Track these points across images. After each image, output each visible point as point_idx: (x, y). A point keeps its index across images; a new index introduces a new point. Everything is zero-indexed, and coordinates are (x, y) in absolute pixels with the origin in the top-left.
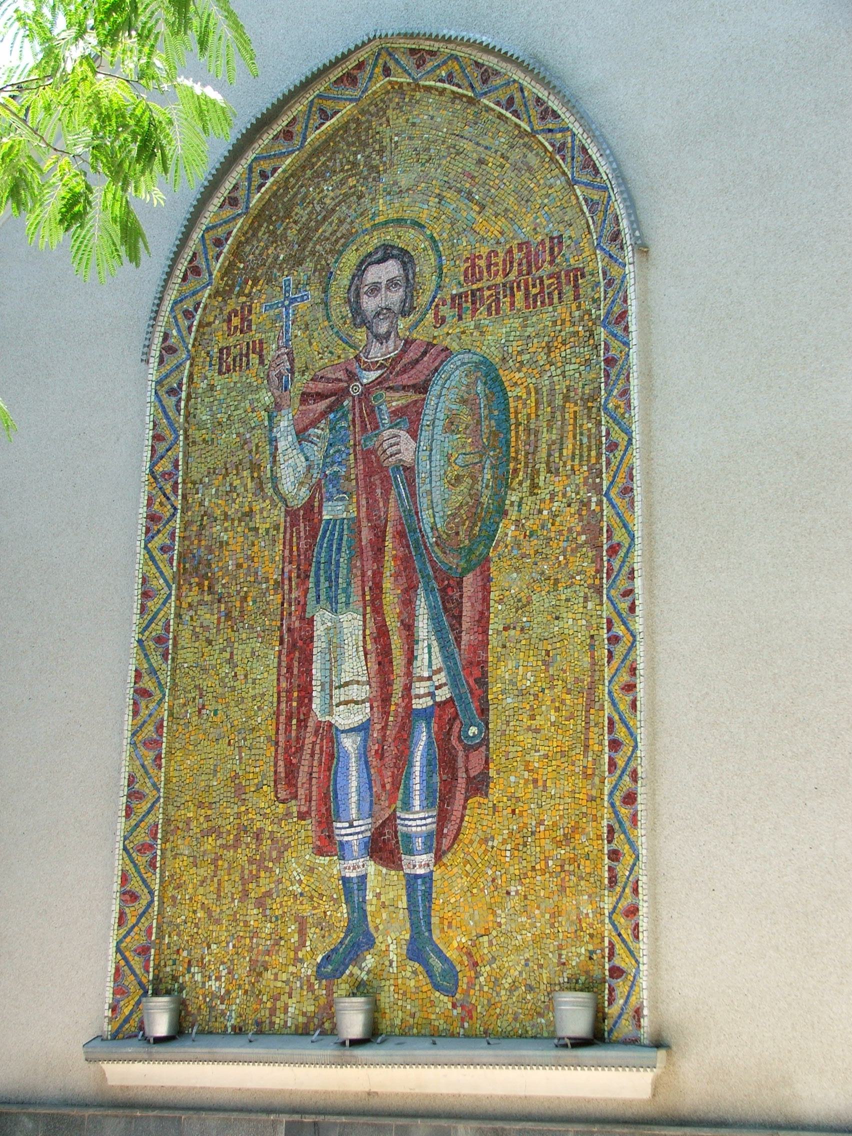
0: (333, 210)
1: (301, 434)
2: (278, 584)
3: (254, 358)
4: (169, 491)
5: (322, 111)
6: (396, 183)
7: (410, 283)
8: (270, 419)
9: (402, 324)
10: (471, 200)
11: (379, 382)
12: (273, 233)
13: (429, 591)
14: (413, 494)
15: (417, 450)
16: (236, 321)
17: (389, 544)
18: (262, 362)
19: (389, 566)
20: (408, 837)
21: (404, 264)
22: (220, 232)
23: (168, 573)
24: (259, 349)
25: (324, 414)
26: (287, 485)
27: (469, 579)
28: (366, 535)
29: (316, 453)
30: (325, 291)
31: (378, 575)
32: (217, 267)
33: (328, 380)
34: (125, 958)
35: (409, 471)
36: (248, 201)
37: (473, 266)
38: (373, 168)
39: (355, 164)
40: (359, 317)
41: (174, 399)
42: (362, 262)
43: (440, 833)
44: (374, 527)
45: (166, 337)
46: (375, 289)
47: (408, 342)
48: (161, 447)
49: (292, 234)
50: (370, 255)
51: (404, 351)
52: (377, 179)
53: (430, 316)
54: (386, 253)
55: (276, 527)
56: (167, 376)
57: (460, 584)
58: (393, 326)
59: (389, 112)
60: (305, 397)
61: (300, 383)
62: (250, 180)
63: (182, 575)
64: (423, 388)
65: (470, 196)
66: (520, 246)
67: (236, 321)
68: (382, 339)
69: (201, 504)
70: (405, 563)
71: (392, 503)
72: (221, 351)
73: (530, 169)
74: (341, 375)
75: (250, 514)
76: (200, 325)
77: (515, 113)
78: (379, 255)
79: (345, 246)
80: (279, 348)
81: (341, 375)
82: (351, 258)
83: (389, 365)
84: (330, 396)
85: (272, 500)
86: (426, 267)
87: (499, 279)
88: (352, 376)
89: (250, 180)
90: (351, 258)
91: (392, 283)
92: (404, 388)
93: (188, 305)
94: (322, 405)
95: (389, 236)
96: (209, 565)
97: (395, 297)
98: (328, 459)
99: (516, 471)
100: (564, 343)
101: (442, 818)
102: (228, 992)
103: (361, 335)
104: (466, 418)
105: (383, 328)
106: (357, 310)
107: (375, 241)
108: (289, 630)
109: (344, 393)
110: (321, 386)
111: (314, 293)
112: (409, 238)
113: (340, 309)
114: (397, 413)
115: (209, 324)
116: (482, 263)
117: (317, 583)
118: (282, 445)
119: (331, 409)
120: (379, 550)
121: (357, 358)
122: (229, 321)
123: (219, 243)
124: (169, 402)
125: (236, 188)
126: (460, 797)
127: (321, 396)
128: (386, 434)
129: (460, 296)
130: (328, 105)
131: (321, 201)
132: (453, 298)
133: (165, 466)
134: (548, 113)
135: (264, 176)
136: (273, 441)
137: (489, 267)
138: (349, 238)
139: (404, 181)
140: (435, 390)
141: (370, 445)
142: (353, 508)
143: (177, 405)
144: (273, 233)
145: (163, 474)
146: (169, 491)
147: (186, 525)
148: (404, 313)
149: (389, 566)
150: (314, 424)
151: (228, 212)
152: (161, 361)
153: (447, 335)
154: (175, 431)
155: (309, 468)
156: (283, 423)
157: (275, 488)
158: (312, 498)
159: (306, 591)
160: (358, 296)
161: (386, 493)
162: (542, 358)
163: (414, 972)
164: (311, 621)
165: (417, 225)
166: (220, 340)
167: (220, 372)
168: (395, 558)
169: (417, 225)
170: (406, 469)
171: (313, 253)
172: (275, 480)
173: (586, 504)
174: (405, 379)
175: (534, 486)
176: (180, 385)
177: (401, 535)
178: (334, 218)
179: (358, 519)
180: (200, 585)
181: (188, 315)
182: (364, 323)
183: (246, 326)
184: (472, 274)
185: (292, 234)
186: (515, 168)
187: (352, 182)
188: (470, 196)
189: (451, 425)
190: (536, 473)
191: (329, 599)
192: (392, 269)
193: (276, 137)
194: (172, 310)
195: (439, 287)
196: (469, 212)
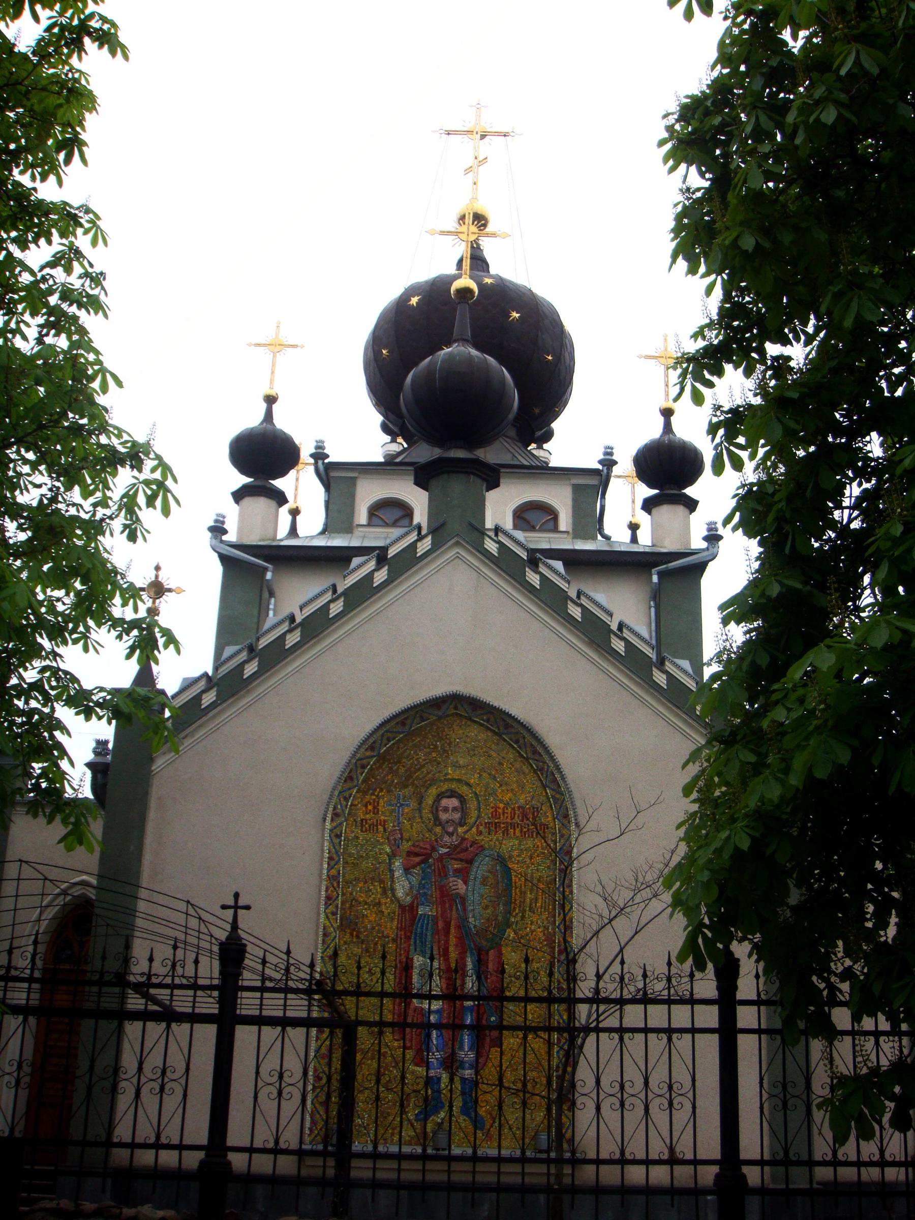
0: (423, 766)
1: (407, 870)
2: (394, 940)
3: (381, 828)
4: (335, 885)
5: (422, 717)
6: (457, 762)
7: (463, 809)
8: (390, 860)
9: (460, 830)
10: (496, 780)
11: (448, 854)
12: (391, 768)
13: (472, 954)
14: (464, 909)
15: (467, 889)
16: (370, 807)
17: (453, 930)
18: (385, 830)
19: (453, 941)
20: (462, 1062)
21: (461, 802)
22: (364, 762)
23: (335, 925)
24: (384, 824)
25: (419, 864)
26: (400, 893)
27: (491, 952)
28: (441, 925)
29: (415, 881)
30: (420, 803)
31: (447, 942)
32: (361, 778)
33: (421, 848)
34: (315, 1107)
35: (463, 900)
36: (380, 749)
37: (496, 811)
38: (445, 751)
39: (436, 747)
40: (437, 821)
41: (338, 840)
42: (439, 795)
43: (477, 1061)
44: (445, 921)
45: (335, 808)
46: (446, 810)
47: (463, 839)
48: (332, 863)
49: (402, 770)
50: (443, 793)
51: (461, 843)
52: (448, 757)
53: (474, 829)
54: (452, 794)
55: (394, 913)
56: (335, 828)
57: (487, 954)
58: (456, 830)
59: (454, 726)
60: (409, 853)
61: (406, 846)
62: (382, 740)
63: (342, 928)
64: (470, 862)
65: (495, 778)
66: (519, 807)
67: (370, 807)
68: (450, 834)
69: (351, 894)
70: (461, 940)
71: (454, 913)
72: (362, 820)
73: (524, 773)
74: (428, 846)
75: (379, 904)
76: (352, 805)
77: (519, 747)
78: (448, 794)
79: (430, 785)
80: (394, 826)
81: (428, 846)
82: (433, 791)
83: (454, 848)
84: (421, 855)
85: (391, 900)
86: (472, 805)
87: (509, 820)
88: (434, 849)
89: (382, 740)
90: (433, 791)
91: (455, 809)
92: (461, 860)
93: (347, 794)
94: (417, 859)
95: (454, 786)
96: (356, 924)
97: (457, 816)
98: (421, 886)
99: (515, 908)
100: (538, 856)
101: (478, 1055)
102: (368, 1125)
103: (438, 830)
104: (491, 880)
105: (451, 829)
106: (437, 819)
107: (445, 787)
108: (400, 962)
109: (429, 856)
110: (417, 850)
111: (413, 804)
112: (463, 790)
113: (426, 813)
114: (457, 871)
115: (356, 805)
116: (500, 811)
117: (415, 943)
118: (397, 874)
119: (422, 862)
120: (447, 932)
121: (436, 840)
122: (366, 806)
123: (363, 767)
124: (337, 841)
125: (374, 742)
126: (487, 1046)
127: (417, 855)
128: (451, 879)
129: (489, 823)
130: (425, 715)
131: (417, 759)
132: (486, 823)
133: (334, 872)
134: (535, 752)
135: (389, 740)
136: (392, 872)
137: (504, 813)
138: (433, 782)
139: (462, 762)
140: (476, 864)
141: (443, 883)
142: (434, 910)
143: (340, 843)
144: (391, 768)
145: (333, 876)
146: (335, 885)
147: (343, 903)
148: (462, 824)
149: (453, 941)
150: (414, 867)
151: (368, 753)
152: (332, 820)
153: (485, 839)
154: (339, 856)
155: (411, 888)
156: (397, 864)
157: (394, 895)
158: (413, 902)
159: (410, 945)
160: (437, 811)
161: (451, 906)
162: (528, 861)
163: (464, 1120)
164: (412, 959)
165: (468, 784)
166: (361, 815)
167: (362, 831)
168: (455, 937)
169: (468, 784)
170: (461, 897)
171: (413, 784)
172: (393, 890)
173: (546, 928)
174: (462, 856)
175: (523, 917)
176: (341, 833)
177: (458, 927)
178: (424, 770)
179: (436, 917)
180: (351, 934)
181: (346, 799)
182: (440, 824)
183: (376, 810)
184: (495, 814)
185: (402, 770)
186: (517, 770)
187: (434, 755)
188: (495, 778)
189: (484, 882)
190: (524, 911)
191: (421, 951)
192: (454, 802)
193: (397, 723)
194: (339, 795)
195: (478, 817)
196: (494, 785)
